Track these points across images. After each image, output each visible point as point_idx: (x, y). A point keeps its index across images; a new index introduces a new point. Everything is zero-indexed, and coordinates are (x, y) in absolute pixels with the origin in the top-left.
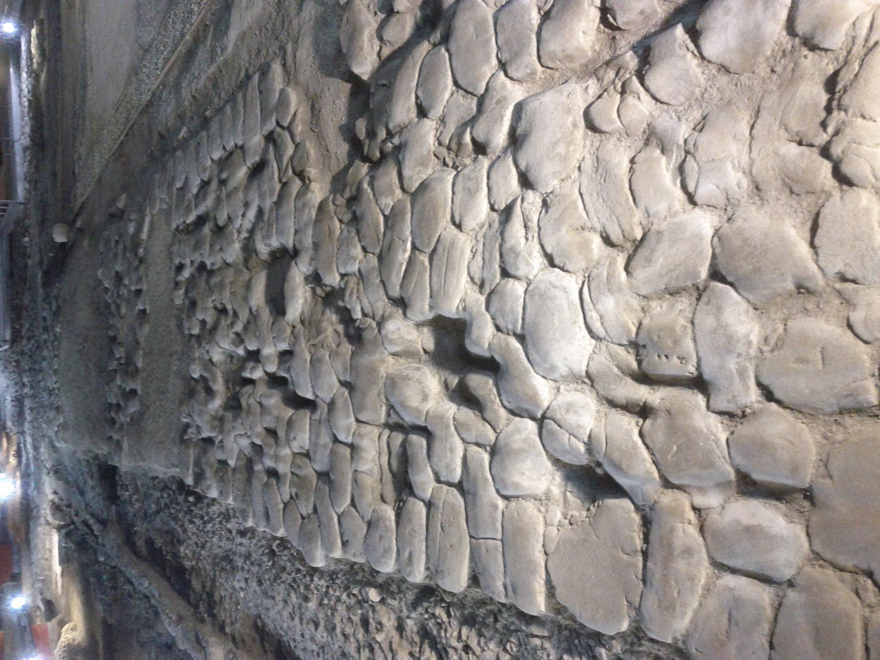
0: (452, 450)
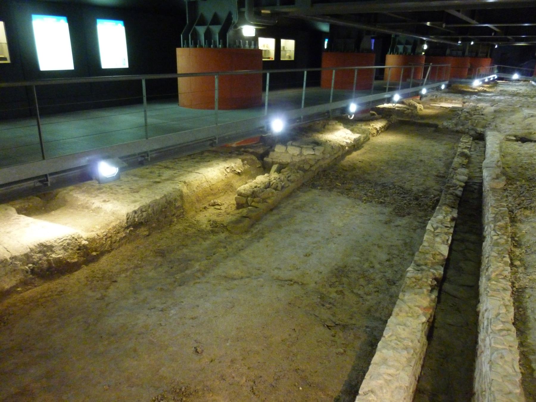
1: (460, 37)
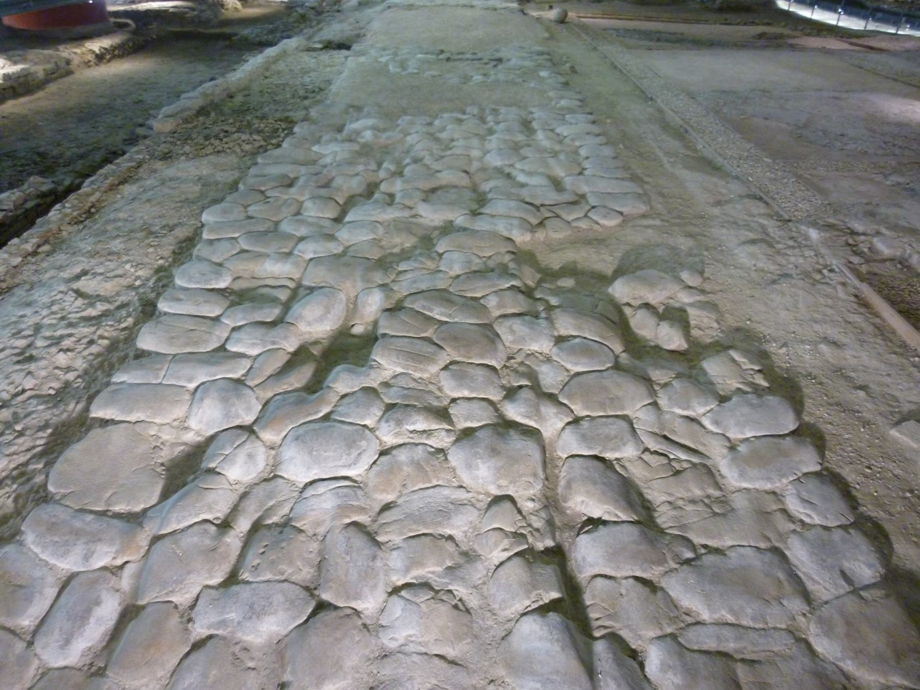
0: (253, 345)
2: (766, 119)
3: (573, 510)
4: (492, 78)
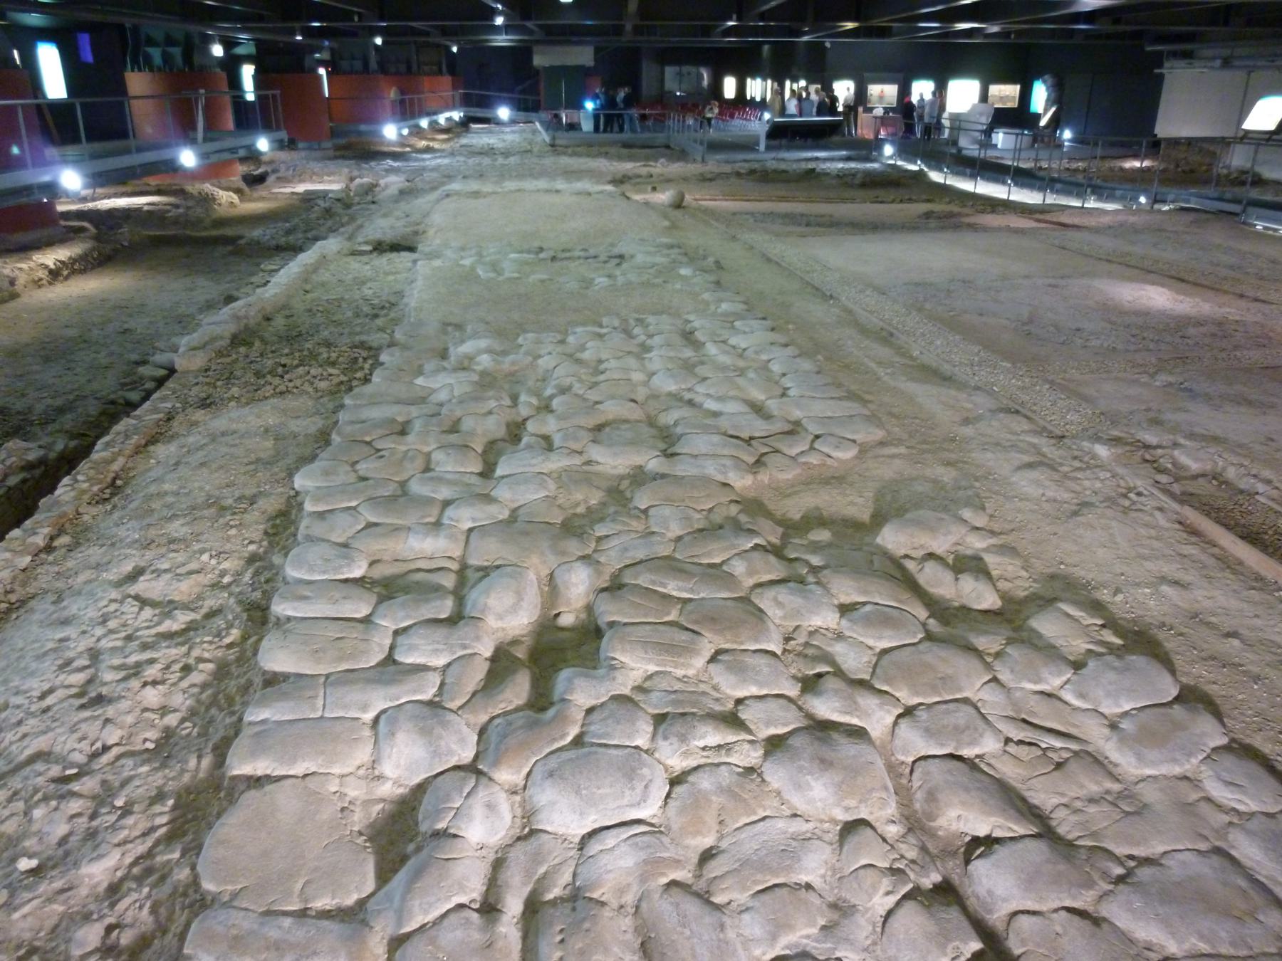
1: (297, 25)
2: (981, 315)
3: (946, 829)
4: (621, 280)
